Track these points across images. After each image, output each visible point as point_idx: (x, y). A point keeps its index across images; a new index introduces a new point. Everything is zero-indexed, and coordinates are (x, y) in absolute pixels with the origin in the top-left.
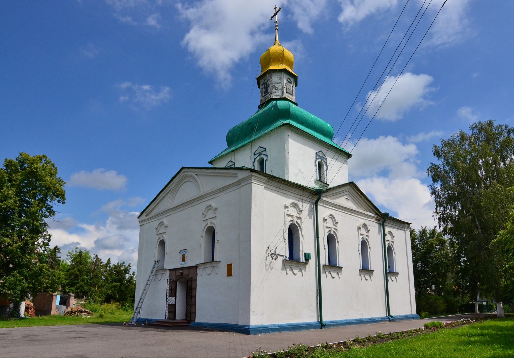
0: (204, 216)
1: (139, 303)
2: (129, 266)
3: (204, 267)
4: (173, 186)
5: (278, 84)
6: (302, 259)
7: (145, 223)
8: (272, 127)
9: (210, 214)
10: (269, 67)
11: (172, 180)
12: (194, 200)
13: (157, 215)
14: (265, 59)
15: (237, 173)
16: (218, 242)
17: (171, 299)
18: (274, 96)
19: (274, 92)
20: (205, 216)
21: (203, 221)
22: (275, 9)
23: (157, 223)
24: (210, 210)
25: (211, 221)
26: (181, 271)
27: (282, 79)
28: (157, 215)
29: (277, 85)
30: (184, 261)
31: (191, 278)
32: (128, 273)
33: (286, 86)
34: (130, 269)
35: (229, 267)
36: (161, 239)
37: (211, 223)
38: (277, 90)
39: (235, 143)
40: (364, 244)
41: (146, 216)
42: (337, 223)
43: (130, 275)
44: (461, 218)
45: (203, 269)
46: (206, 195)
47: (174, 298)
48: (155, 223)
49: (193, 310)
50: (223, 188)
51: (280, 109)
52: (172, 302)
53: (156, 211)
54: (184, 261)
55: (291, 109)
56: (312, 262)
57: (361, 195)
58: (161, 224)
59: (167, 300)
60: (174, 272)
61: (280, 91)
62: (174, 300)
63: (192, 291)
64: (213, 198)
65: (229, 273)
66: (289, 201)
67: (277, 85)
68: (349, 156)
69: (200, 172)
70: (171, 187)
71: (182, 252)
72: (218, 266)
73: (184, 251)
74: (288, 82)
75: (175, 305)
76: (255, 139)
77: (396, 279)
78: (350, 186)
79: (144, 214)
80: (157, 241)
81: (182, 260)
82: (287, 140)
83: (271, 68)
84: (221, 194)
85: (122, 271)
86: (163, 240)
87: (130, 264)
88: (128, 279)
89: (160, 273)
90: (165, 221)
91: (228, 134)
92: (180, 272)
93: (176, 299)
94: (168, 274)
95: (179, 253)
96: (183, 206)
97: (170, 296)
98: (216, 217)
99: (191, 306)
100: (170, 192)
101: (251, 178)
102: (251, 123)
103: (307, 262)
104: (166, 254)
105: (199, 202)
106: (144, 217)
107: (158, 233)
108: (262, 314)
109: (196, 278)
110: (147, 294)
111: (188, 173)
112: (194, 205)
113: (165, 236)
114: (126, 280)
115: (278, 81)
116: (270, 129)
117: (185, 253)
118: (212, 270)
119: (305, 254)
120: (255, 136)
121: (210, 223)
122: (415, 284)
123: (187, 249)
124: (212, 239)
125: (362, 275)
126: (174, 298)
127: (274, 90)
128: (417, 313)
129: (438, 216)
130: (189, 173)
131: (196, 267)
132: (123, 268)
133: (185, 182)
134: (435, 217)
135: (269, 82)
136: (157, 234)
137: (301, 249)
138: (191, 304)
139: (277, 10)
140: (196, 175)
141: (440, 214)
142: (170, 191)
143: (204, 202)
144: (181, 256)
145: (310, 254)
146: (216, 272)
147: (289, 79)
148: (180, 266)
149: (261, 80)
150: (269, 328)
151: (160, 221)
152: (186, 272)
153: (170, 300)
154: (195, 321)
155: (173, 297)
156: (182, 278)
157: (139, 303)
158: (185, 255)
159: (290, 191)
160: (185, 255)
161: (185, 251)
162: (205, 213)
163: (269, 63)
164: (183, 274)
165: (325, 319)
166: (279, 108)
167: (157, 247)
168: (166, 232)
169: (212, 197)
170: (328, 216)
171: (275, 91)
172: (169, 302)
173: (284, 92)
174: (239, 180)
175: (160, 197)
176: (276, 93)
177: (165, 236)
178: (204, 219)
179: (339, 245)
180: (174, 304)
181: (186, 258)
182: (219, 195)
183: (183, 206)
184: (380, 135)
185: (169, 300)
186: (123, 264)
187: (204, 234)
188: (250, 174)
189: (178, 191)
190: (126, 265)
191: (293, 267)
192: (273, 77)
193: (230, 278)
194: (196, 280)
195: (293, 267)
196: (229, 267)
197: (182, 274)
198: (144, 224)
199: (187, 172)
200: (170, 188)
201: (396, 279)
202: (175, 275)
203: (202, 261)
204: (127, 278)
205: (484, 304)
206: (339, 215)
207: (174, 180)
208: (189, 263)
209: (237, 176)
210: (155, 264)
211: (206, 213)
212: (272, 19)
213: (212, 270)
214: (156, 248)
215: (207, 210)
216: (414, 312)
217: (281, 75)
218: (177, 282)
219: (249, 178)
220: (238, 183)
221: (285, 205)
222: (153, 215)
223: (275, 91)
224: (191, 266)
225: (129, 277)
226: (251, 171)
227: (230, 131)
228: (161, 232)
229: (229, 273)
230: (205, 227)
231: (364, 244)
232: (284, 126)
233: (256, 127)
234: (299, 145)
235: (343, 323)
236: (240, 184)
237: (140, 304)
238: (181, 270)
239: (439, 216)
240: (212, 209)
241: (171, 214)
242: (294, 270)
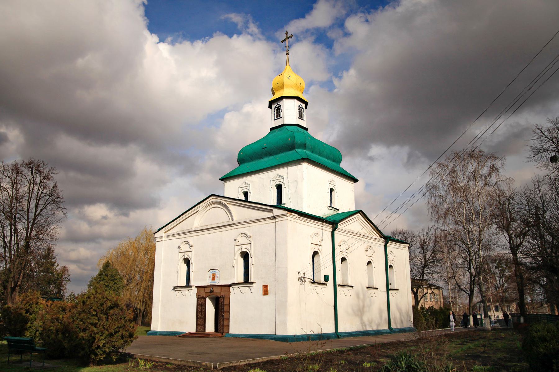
12: (242, 223)
35: (266, 287)
41: (165, 233)
44: (452, 251)
46: (239, 223)
48: (177, 241)
60: (202, 290)
65: (266, 293)
68: (355, 180)
77: (250, 289)
79: (162, 231)
94: (194, 290)
103: (326, 283)
119: (325, 276)
123: (217, 269)
145: (328, 276)
150: (301, 337)
152: (216, 290)
165: (340, 330)
170: (313, 234)
184: (150, 21)
196: (266, 287)
201: (250, 289)
202: (205, 292)
205: (478, 318)
206: (351, 241)
208: (221, 282)
229: (266, 293)
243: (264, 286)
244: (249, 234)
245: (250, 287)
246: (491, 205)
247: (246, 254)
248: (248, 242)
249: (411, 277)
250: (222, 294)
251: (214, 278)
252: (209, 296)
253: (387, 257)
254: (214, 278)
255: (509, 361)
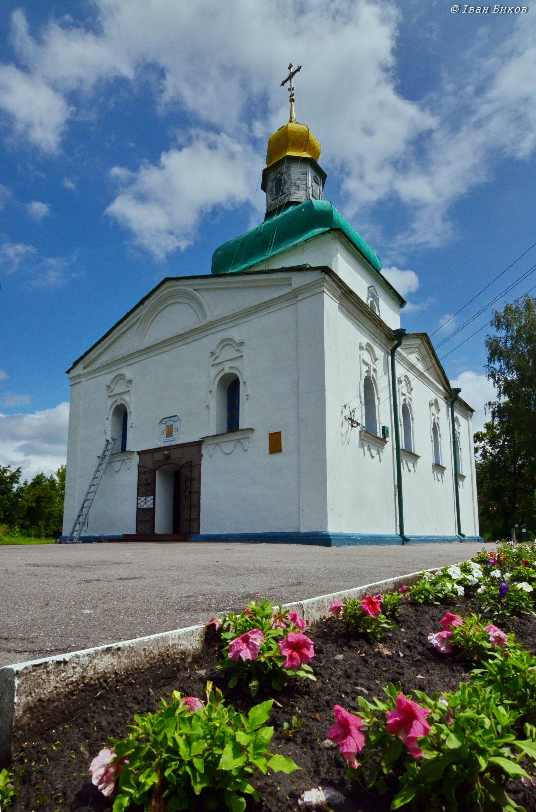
0: (214, 357)
1: (82, 508)
2: (18, 471)
3: (217, 441)
4: (144, 312)
5: (301, 182)
6: (380, 434)
7: (82, 380)
8: (305, 236)
9: (229, 353)
10: (286, 152)
11: (142, 302)
12: (191, 331)
13: (108, 365)
14: (278, 140)
15: (291, 278)
16: (247, 399)
17: (146, 499)
18: (293, 199)
19: (294, 193)
20: (217, 357)
21: (213, 365)
22: (290, 68)
23: (110, 377)
24: (228, 348)
25: (230, 364)
26: (165, 452)
27: (306, 174)
28: (108, 365)
29: (298, 182)
30: (171, 436)
31: (189, 462)
32: (17, 482)
33: (312, 186)
34: (20, 475)
36: (119, 404)
37: (230, 367)
38: (298, 190)
39: (233, 265)
40: (435, 429)
41: (85, 368)
42: (412, 389)
43: (19, 485)
45: (214, 445)
46: (218, 321)
47: (152, 497)
48: (107, 378)
49: (194, 516)
50: (257, 307)
51: (317, 211)
52: (148, 504)
53: (105, 359)
54: (171, 436)
55: (334, 214)
56: (390, 439)
57: (432, 357)
58: (118, 379)
59: (139, 502)
61: (303, 192)
62: (152, 502)
63: (191, 483)
64: (235, 326)
66: (365, 340)
67: (298, 182)
69: (203, 284)
70: (140, 314)
71: (165, 421)
72: (249, 437)
73: (170, 419)
74: (315, 181)
75: (152, 511)
76: (274, 256)
78: (421, 339)
79: (80, 366)
80: (109, 407)
81: (165, 435)
82: (335, 256)
83: (289, 153)
84: (251, 318)
85: (7, 478)
86: (122, 404)
87: (20, 468)
88: (17, 491)
89: (116, 460)
90: (128, 373)
91: (215, 253)
92: (164, 454)
93: (154, 499)
94: (136, 459)
95: (160, 423)
96: (167, 344)
97: (146, 495)
98: (241, 356)
99: (190, 509)
100: (138, 324)
101: (322, 284)
102: (261, 233)
104: (131, 427)
105: (202, 335)
106: (79, 370)
107: (112, 394)
108: (341, 515)
109: (200, 462)
110: (97, 493)
111: (176, 288)
112: (190, 341)
113: (126, 397)
114: (13, 494)
115: (300, 175)
116: (302, 239)
117: (172, 422)
118: (235, 446)
120: (272, 251)
121: (228, 368)
122: (479, 493)
123: (176, 416)
124: (226, 397)
125: (435, 473)
126: (152, 497)
127: (293, 190)
128: (480, 535)
129: (491, 410)
130: (180, 288)
131: (199, 444)
132: (8, 474)
133: (168, 306)
134: (488, 411)
135: (285, 177)
136: (109, 397)
137: (377, 419)
138: (190, 505)
139: (293, 70)
140: (195, 290)
141: (494, 407)
142: (138, 320)
143: (213, 333)
144: (164, 427)
146: (245, 449)
147: (316, 176)
148: (161, 444)
149: (270, 173)
151: (118, 373)
152: (175, 454)
153: (144, 501)
154: (199, 533)
155: (149, 496)
156: (168, 464)
157: (82, 508)
158: (172, 425)
159: (364, 324)
160: (172, 425)
161: (173, 419)
162: (217, 353)
163: (285, 148)
164: (171, 458)
165: (406, 533)
166: (316, 208)
167: (110, 417)
168: (129, 391)
169: (232, 324)
171: (295, 191)
172: (142, 504)
173: (309, 194)
174: (294, 290)
175: (116, 333)
176: (297, 195)
177: (126, 397)
178: (215, 362)
179: (413, 423)
180: (151, 508)
181: (174, 430)
182: (247, 320)
183: (167, 344)
185: (142, 501)
186: (9, 469)
187: (215, 388)
188: (322, 277)
189: (152, 321)
190: (13, 469)
191: (371, 445)
192: (292, 169)
193: (276, 457)
194: (200, 465)
195: (371, 445)
197: (168, 457)
198: (80, 382)
199: (176, 286)
200: (137, 318)
203: (213, 432)
204: (14, 490)
207: (146, 303)
209: (291, 284)
210: (107, 445)
211: (218, 353)
212: (283, 84)
213: (235, 446)
214: (107, 419)
215: (221, 347)
216: (478, 534)
217: (304, 167)
218: (157, 471)
219: (318, 284)
220: (294, 295)
221: (360, 343)
222: (100, 365)
223: (295, 191)
224: (193, 441)
225: (18, 488)
226: (322, 271)
227: (218, 249)
228: (117, 391)
230: (216, 377)
231: (435, 429)
232: (330, 233)
233: (273, 238)
234: (350, 267)
235: (422, 540)
236: (297, 297)
237: (84, 509)
238: (166, 450)
239: (493, 410)
240: (233, 344)
241: (138, 360)
242: (372, 450)
243: (271, 435)
244: (237, 338)
245: (241, 440)
246: (335, 672)
247: (235, 380)
248: (238, 355)
249: (304, 678)
250: (186, 460)
251: (170, 432)
252: (159, 467)
253: (318, 165)
254: (170, 432)
255: (272, 192)
